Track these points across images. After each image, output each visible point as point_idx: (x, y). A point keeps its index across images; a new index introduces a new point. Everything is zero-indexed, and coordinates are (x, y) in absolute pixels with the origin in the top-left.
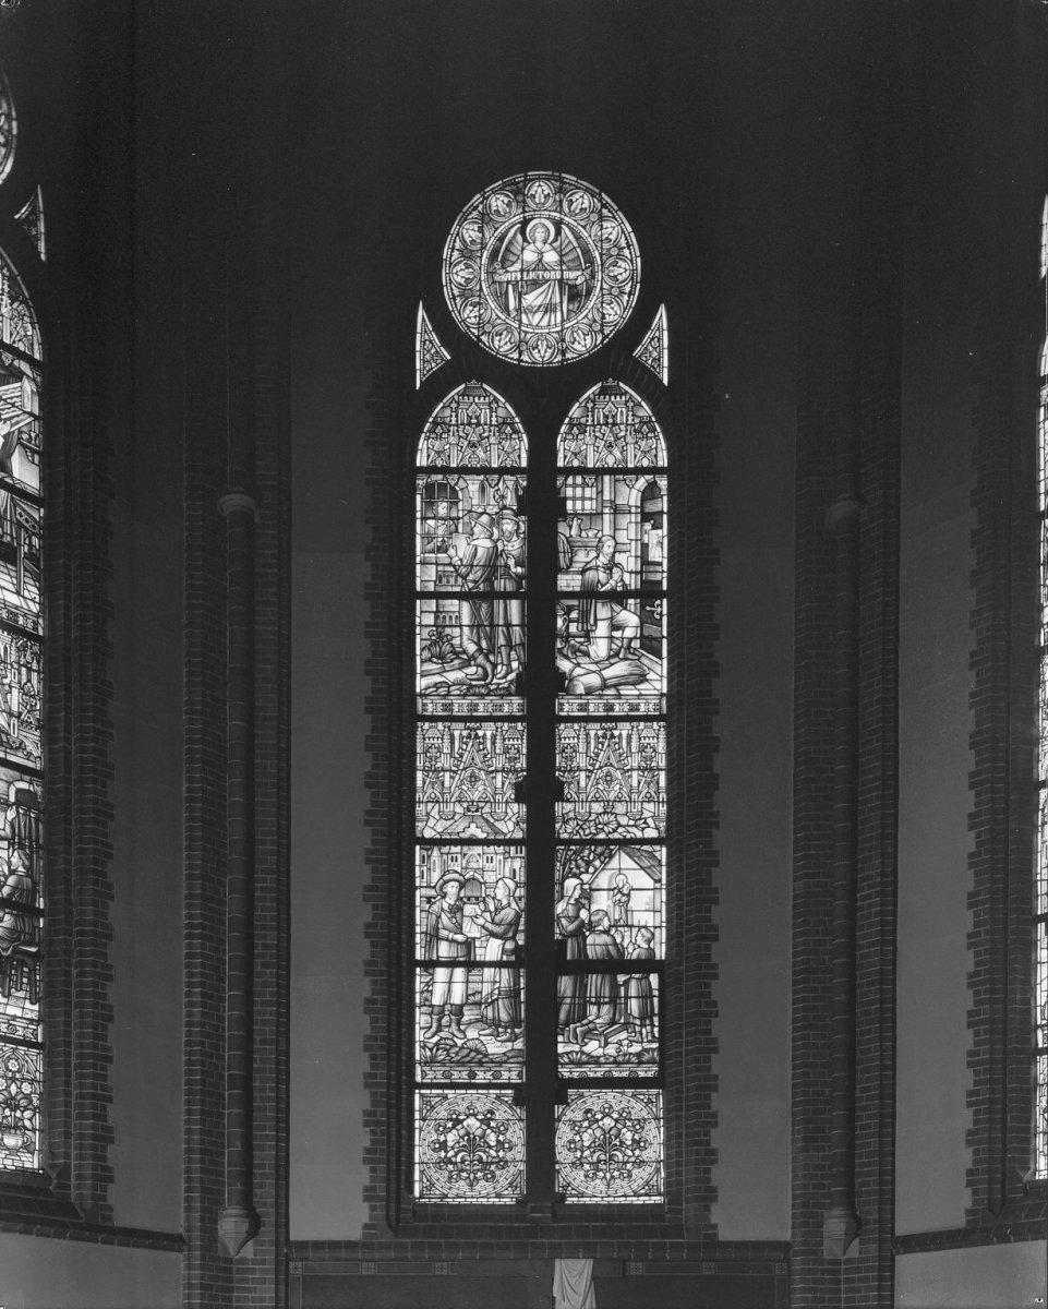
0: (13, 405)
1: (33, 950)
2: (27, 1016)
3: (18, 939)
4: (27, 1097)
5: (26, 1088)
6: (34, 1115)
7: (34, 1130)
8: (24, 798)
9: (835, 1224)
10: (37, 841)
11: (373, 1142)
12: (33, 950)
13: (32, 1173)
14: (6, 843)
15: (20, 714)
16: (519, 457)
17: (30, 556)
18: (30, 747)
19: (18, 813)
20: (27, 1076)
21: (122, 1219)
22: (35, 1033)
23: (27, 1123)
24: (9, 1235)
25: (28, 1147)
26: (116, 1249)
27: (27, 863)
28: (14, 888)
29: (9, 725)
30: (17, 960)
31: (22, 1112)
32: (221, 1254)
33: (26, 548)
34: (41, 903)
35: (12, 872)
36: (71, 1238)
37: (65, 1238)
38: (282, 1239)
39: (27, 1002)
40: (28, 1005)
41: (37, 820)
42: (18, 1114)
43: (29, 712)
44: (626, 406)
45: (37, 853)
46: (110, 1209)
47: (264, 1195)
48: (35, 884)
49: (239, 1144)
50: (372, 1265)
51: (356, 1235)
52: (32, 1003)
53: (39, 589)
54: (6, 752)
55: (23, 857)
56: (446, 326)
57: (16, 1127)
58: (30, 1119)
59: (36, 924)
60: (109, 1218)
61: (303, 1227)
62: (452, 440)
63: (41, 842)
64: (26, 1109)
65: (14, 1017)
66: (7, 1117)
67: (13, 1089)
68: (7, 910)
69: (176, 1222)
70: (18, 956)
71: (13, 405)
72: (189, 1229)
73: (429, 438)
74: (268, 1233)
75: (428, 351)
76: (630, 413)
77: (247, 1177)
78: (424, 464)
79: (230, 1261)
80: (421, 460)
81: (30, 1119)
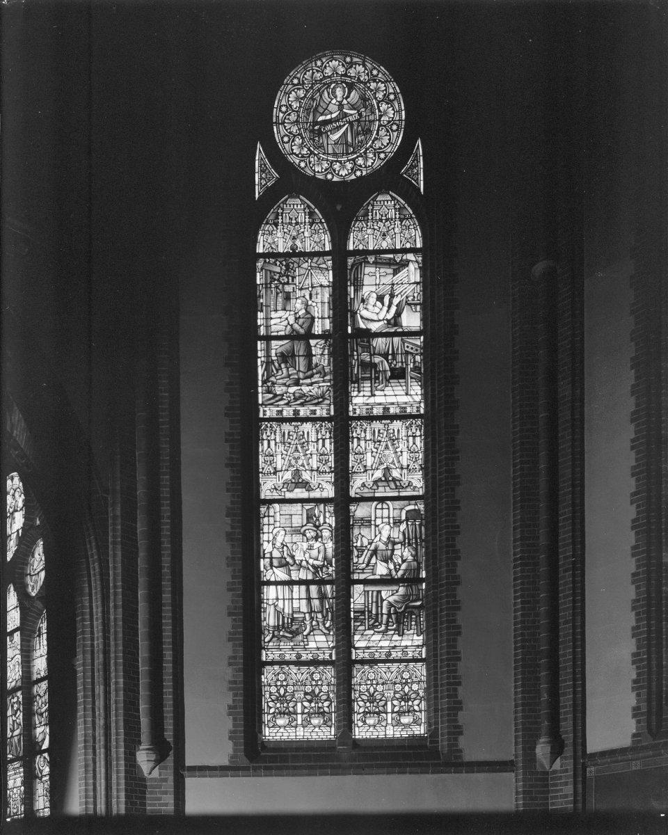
0: (402, 284)
1: (419, 603)
2: (415, 644)
3: (407, 601)
4: (416, 692)
5: (415, 687)
6: (421, 702)
7: (420, 711)
8: (412, 516)
9: (542, 750)
10: (421, 537)
11: (638, 674)
12: (419, 603)
13: (420, 738)
14: (400, 545)
15: (408, 466)
16: (324, 245)
17: (415, 369)
18: (415, 483)
19: (407, 525)
20: (415, 680)
21: (469, 756)
22: (331, 655)
23: (416, 708)
24: (392, 776)
25: (416, 722)
26: (464, 775)
27: (414, 553)
28: (406, 570)
29: (401, 475)
30: (408, 612)
31: (413, 702)
32: (539, 769)
33: (412, 364)
34: (423, 574)
35: (404, 561)
36: (433, 773)
37: (428, 773)
38: (580, 753)
39: (415, 635)
40: (415, 637)
41: (420, 525)
42: (410, 703)
43: (414, 462)
44: (385, 205)
45: (421, 545)
46: (461, 751)
47: (566, 726)
48: (419, 564)
49: (545, 695)
50: (638, 762)
51: (626, 742)
52: (418, 636)
53: (420, 386)
54: (399, 492)
55: (411, 550)
56: (276, 157)
57: (409, 711)
58: (418, 705)
59: (420, 588)
60: (460, 757)
61: (597, 741)
62: (369, 231)
63: (423, 537)
64: (415, 699)
65: (406, 647)
66: (402, 706)
67: (407, 689)
68: (401, 585)
69: (509, 751)
70: (408, 610)
71: (402, 284)
72: (516, 756)
73: (264, 234)
74: (569, 751)
75: (262, 178)
76: (397, 213)
77: (555, 719)
78: (261, 251)
79: (547, 773)
80: (260, 249)
81: (418, 705)
